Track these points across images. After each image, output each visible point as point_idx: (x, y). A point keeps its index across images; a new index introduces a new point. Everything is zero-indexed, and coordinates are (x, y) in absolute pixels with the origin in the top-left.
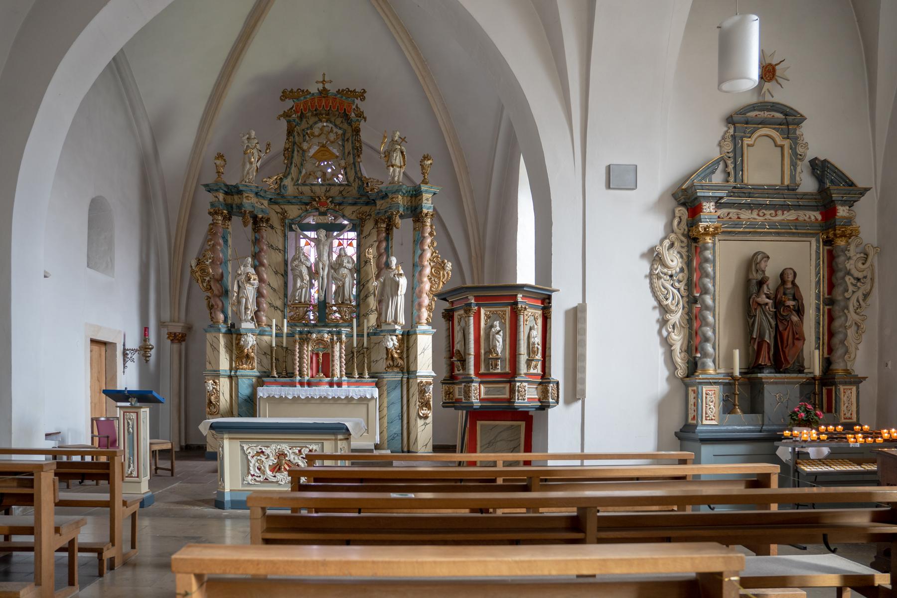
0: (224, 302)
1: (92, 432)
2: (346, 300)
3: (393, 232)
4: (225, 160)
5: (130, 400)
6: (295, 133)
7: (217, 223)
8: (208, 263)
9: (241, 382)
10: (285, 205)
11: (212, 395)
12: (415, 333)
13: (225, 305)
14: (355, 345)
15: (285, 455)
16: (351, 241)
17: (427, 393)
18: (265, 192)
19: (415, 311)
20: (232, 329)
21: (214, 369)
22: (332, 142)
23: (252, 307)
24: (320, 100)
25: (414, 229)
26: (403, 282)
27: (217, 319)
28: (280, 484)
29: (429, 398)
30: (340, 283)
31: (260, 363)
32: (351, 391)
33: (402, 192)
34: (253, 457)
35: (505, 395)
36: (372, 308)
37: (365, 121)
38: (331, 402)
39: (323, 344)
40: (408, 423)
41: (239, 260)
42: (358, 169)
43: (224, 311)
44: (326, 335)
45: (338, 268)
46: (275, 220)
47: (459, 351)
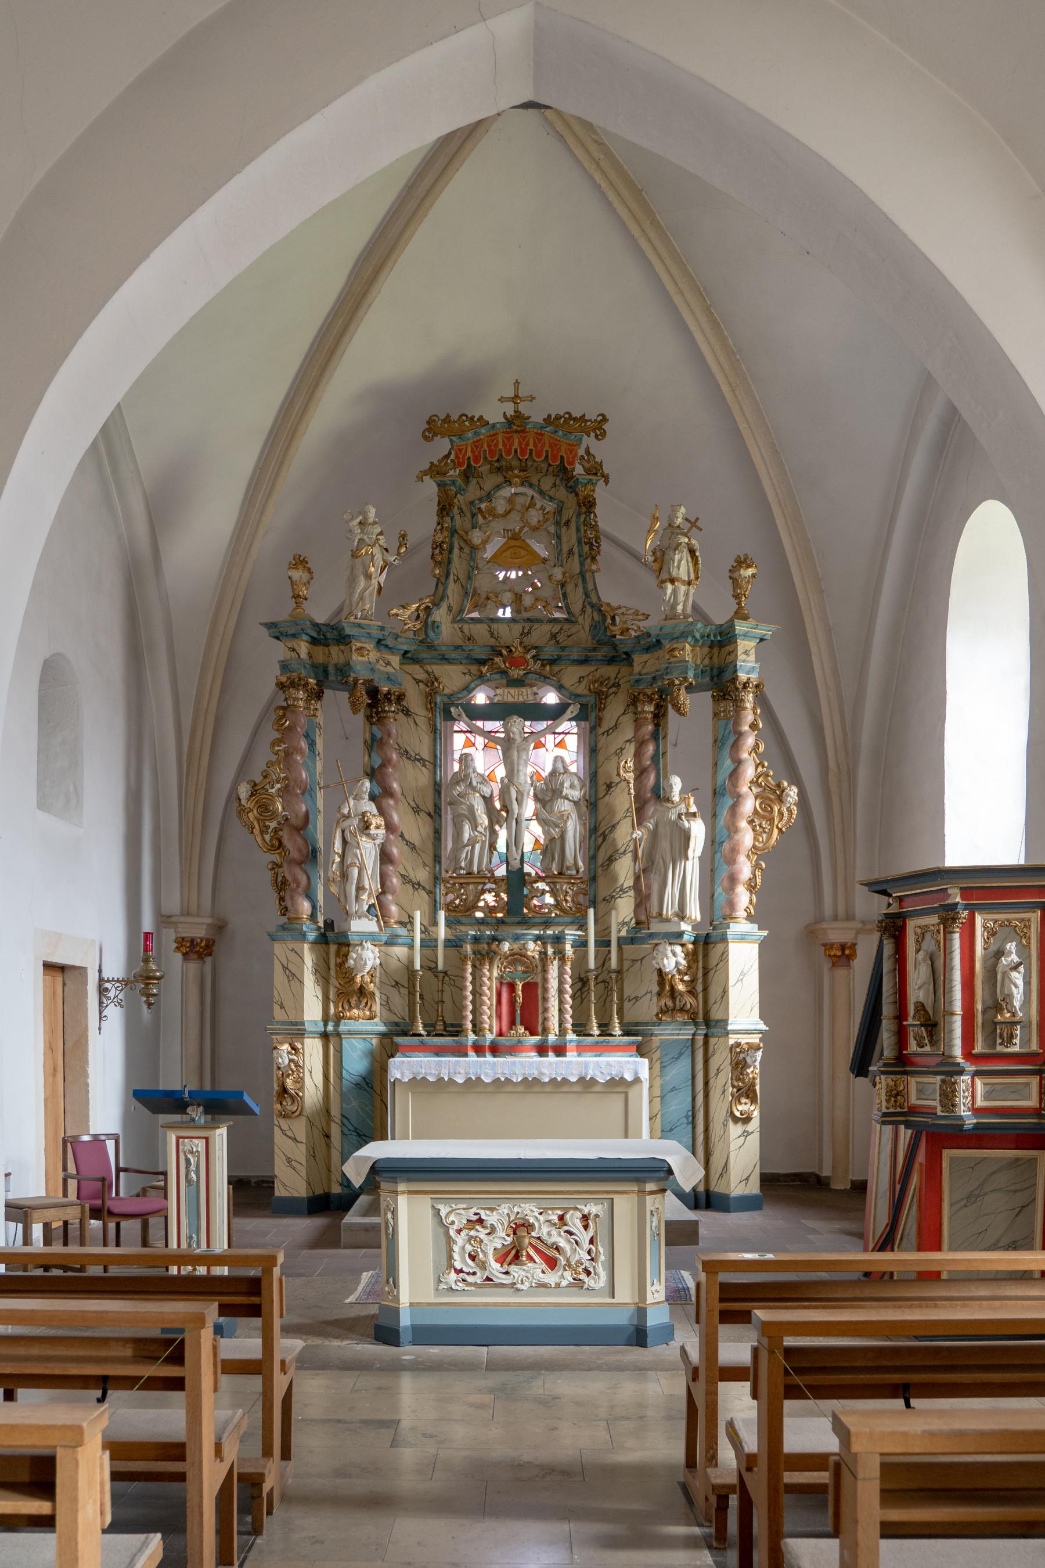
1: (65, 1169)
2: (568, 868)
3: (667, 719)
4: (309, 571)
5: (189, 1110)
6: (456, 511)
7: (296, 706)
8: (273, 791)
10: (435, 664)
11: (288, 1076)
12: (724, 939)
13: (312, 883)
14: (592, 965)
15: (529, 1227)
16: (562, 736)
17: (749, 1067)
18: (397, 637)
19: (719, 890)
20: (329, 934)
21: (292, 1019)
22: (535, 529)
23: (372, 883)
24: (508, 439)
25: (716, 715)
26: (698, 830)
27: (297, 911)
28: (518, 1290)
29: (754, 1078)
31: (387, 1004)
32: (592, 1066)
33: (694, 637)
34: (459, 1231)
35: (1028, 1099)
36: (622, 885)
37: (607, 482)
38: (548, 1089)
39: (523, 964)
40: (706, 1130)
41: (341, 790)
42: (590, 587)
44: (531, 945)
45: (551, 800)
46: (414, 699)
47: (923, 1005)
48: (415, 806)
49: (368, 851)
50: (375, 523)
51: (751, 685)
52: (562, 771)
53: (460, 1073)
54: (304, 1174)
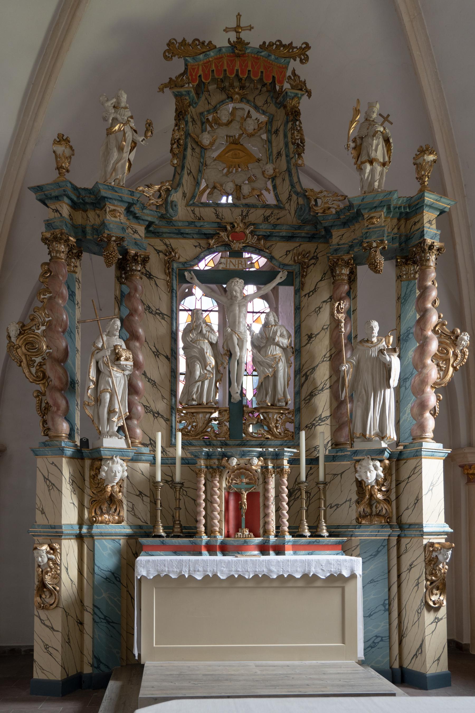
0: (68, 399)
2: (279, 401)
6: (189, 118)
7: (59, 258)
8: (39, 331)
9: (99, 546)
10: (171, 238)
11: (47, 573)
13: (71, 408)
14: (303, 478)
20: (85, 451)
21: (51, 523)
25: (399, 277)
27: (57, 430)
30: (269, 372)
31: (132, 510)
37: (309, 95)
38: (275, 584)
42: (295, 179)
43: (69, 419)
44: (255, 461)
48: (155, 350)
49: (118, 379)
50: (126, 108)
51: (435, 248)
52: (273, 324)
53: (198, 571)
54: (59, 658)
